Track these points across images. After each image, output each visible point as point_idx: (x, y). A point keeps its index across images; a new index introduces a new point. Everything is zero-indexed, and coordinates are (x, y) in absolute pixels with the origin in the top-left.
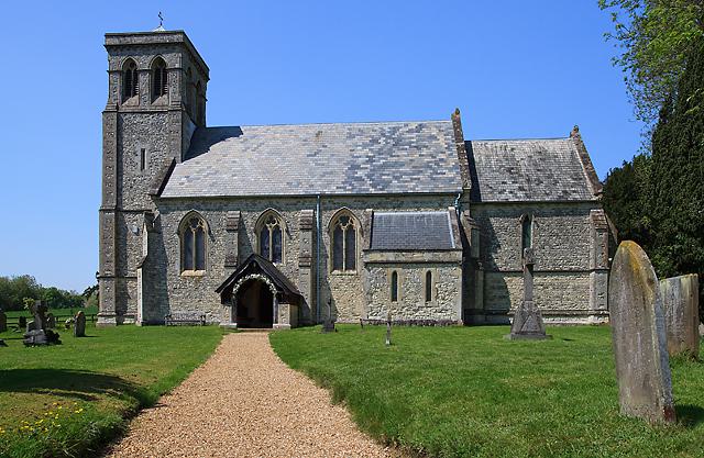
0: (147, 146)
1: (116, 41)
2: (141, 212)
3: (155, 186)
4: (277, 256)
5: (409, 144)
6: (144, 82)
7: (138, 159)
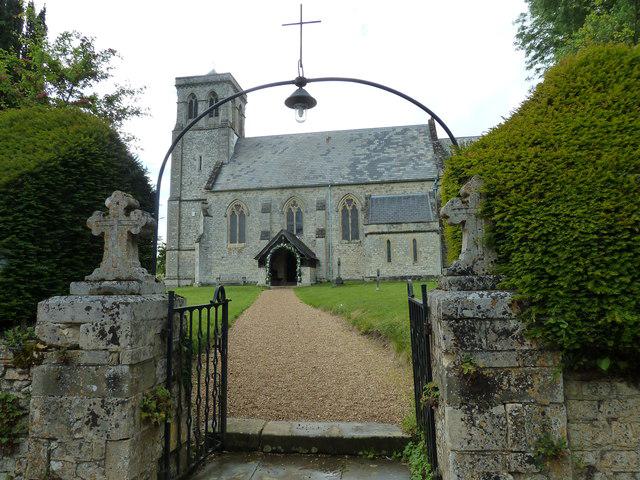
4: (300, 230)
7: (197, 163)
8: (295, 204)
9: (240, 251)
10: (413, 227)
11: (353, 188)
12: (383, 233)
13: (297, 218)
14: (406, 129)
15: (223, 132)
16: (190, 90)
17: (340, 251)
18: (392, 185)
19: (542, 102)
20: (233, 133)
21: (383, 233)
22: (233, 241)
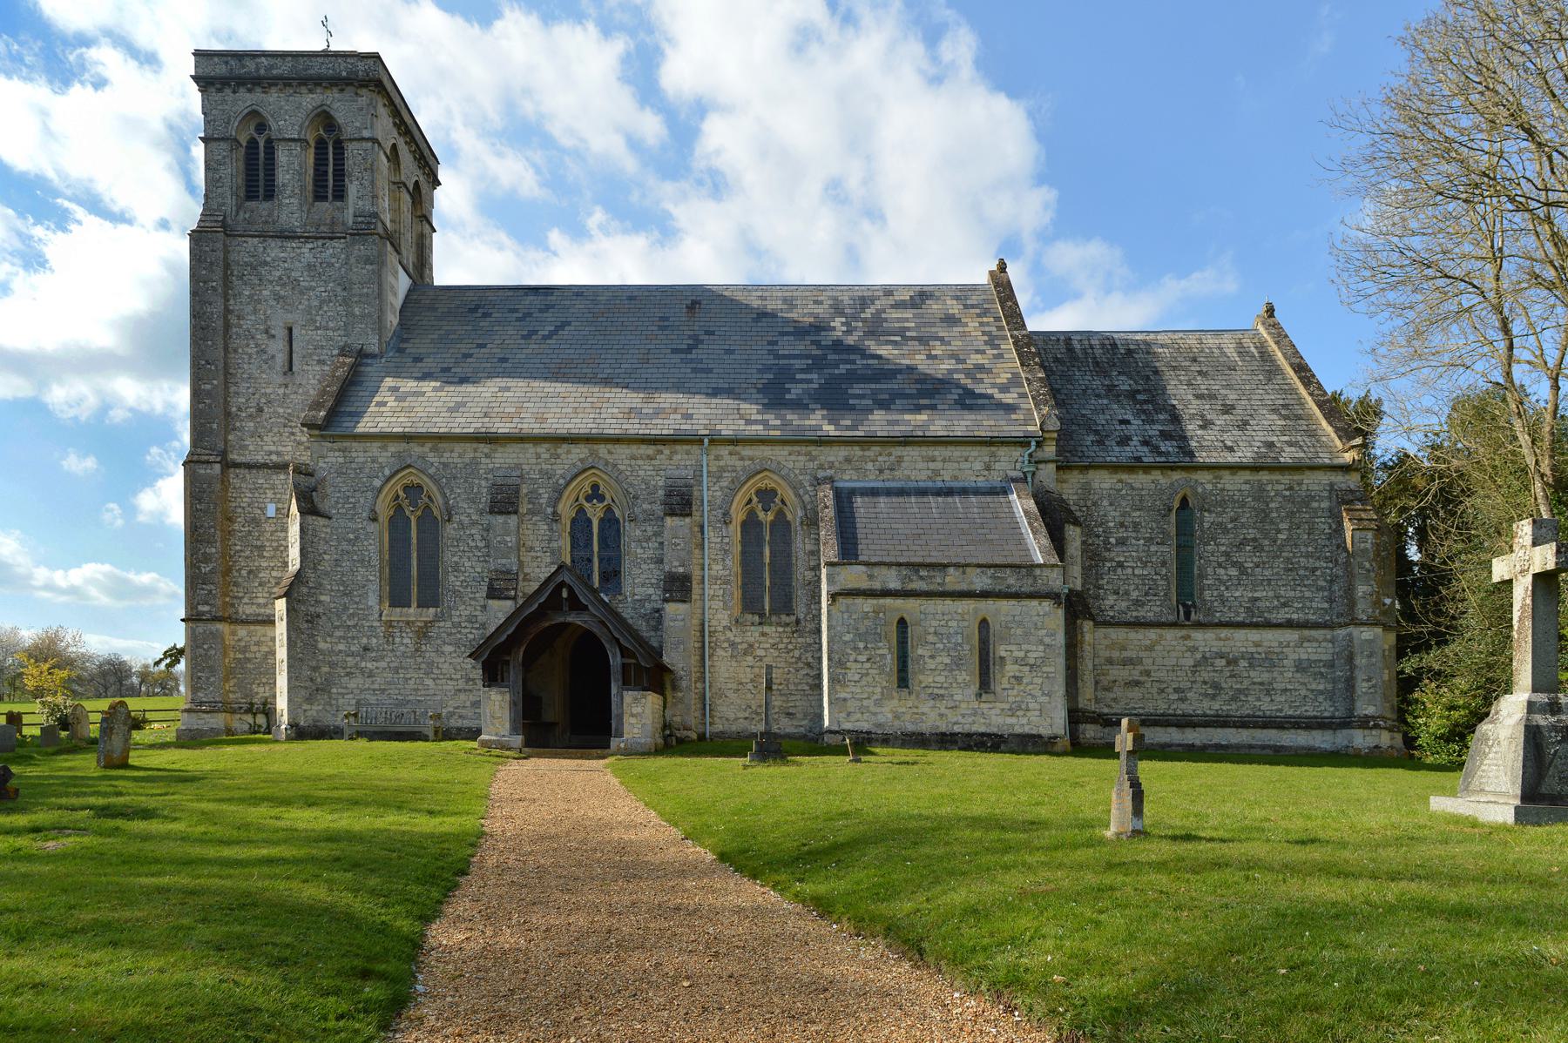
0: (295, 318)
1: (221, 69)
2: (282, 467)
3: (316, 405)
4: (612, 575)
5: (902, 332)
6: (292, 166)
7: (277, 347)
8: (595, 494)
9: (423, 634)
10: (980, 581)
11: (780, 453)
12: (886, 593)
13: (602, 540)
14: (922, 296)
15: (360, 249)
16: (246, 100)
17: (733, 645)
18: (898, 451)
19: (135, 493)
20: (392, 258)
21: (886, 593)
22: (398, 599)
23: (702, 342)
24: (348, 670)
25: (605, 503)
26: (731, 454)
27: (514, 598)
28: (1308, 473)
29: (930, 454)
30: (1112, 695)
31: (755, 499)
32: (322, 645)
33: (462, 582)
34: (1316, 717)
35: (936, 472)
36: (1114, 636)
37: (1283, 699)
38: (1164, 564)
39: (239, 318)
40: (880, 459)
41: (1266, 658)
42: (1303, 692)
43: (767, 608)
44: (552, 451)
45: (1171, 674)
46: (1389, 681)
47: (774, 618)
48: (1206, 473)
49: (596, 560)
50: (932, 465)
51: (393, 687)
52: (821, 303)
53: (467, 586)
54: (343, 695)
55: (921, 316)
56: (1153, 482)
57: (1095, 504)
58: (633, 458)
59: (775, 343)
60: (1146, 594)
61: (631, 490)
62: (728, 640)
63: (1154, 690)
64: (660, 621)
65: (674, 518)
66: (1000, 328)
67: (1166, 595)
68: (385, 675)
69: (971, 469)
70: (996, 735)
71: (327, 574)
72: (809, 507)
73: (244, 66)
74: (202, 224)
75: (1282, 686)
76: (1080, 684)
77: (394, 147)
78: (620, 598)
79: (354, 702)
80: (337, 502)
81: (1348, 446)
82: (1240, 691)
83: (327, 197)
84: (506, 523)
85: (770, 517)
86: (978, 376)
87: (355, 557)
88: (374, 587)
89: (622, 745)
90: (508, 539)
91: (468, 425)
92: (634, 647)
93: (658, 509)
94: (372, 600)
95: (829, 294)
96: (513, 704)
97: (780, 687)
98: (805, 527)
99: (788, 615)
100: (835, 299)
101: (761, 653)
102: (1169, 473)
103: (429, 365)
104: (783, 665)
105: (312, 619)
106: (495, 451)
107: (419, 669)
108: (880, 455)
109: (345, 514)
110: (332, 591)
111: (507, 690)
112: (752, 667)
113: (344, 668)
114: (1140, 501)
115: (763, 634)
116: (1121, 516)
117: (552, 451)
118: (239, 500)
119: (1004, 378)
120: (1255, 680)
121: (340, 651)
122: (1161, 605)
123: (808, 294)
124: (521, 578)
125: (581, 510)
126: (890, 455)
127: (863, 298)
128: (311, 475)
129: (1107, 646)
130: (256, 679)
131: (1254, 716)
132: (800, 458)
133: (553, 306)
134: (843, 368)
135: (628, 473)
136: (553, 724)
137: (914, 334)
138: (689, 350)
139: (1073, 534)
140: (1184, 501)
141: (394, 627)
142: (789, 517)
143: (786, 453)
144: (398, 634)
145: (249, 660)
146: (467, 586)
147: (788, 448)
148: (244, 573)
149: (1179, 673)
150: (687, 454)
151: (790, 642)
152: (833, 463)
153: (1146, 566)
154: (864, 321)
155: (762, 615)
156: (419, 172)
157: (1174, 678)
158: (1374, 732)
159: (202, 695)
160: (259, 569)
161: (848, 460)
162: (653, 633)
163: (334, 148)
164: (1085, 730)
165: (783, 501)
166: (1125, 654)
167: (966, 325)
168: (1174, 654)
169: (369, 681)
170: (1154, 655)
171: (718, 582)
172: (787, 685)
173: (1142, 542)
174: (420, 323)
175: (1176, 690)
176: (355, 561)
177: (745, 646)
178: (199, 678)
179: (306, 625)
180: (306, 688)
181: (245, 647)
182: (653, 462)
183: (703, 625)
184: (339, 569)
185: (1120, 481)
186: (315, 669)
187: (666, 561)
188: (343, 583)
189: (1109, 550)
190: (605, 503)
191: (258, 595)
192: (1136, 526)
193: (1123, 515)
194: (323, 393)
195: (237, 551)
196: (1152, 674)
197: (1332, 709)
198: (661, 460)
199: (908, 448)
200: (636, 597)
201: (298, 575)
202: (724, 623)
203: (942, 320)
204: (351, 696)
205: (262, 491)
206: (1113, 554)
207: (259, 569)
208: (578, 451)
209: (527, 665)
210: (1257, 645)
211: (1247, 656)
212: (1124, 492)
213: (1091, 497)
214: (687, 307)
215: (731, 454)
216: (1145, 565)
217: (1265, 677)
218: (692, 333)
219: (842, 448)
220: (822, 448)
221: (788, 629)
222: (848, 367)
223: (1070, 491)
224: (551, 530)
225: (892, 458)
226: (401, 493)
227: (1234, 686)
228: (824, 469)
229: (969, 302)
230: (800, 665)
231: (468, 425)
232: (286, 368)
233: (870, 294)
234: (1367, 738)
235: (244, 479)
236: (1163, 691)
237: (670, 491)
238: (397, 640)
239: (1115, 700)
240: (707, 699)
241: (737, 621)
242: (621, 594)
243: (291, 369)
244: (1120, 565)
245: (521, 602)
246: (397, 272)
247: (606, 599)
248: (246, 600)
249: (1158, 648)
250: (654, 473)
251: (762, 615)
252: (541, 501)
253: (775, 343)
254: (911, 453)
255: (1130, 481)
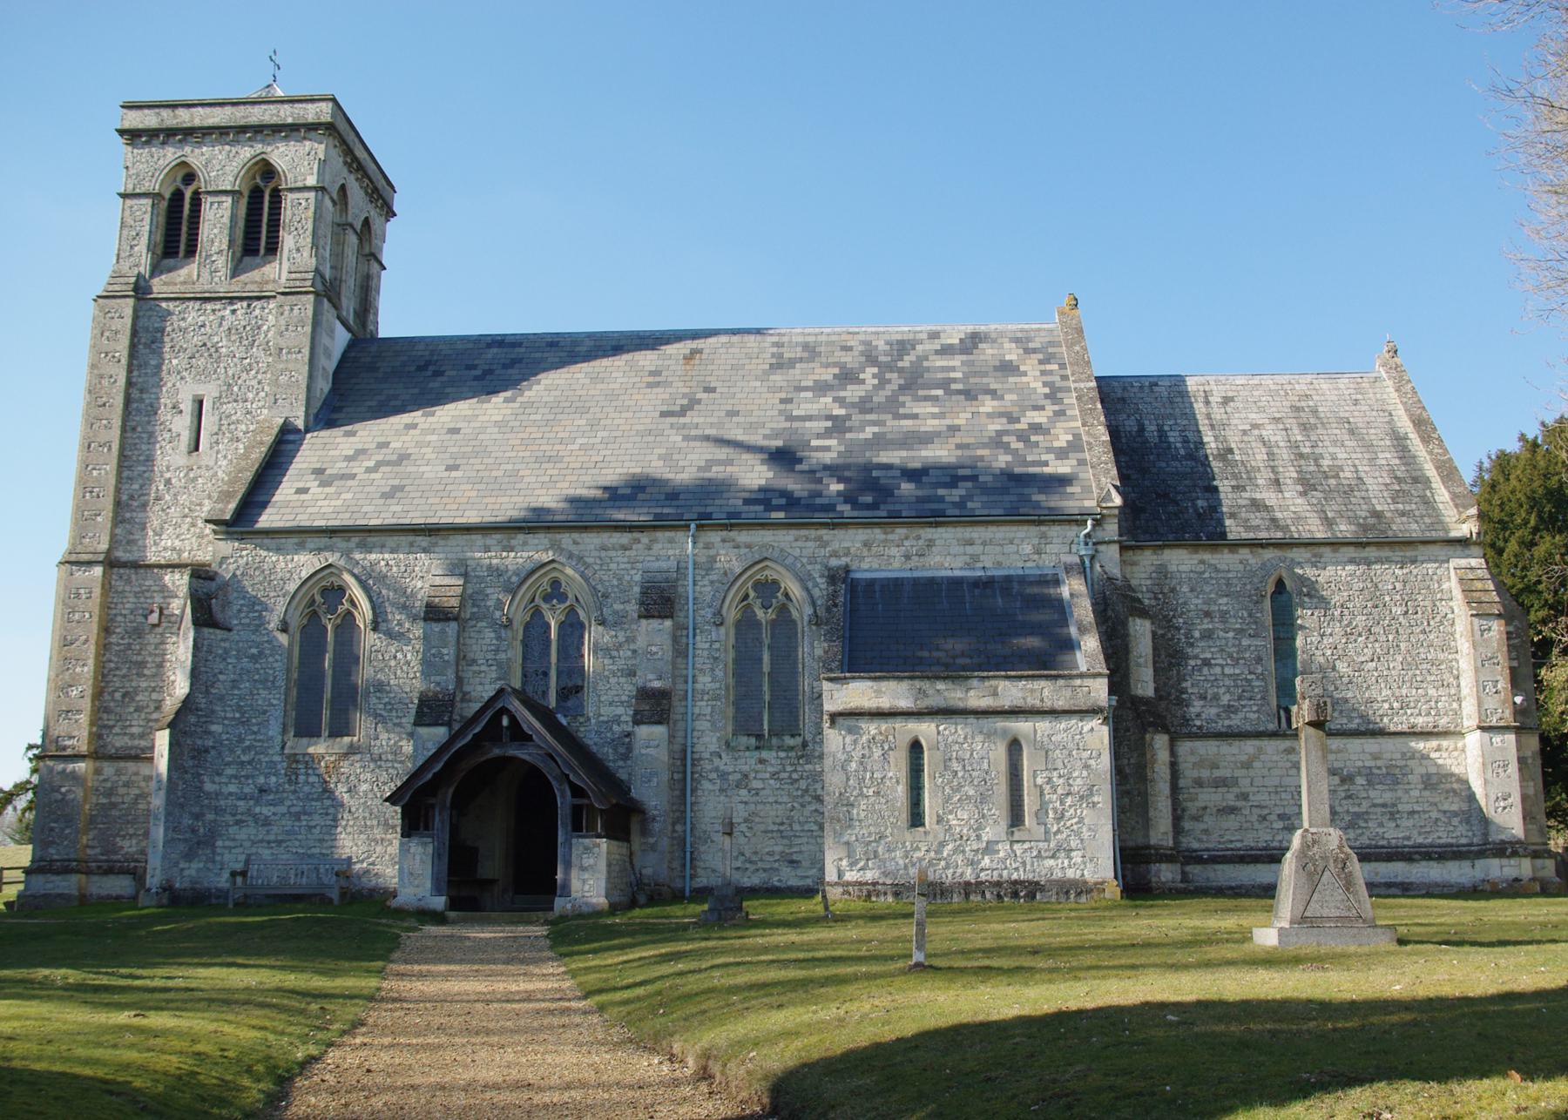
5: (945, 384)
17: (723, 776)
23: (699, 402)
24: (239, 817)
25: (568, 603)
26: (724, 541)
27: (449, 724)
28: (1421, 548)
29: (967, 535)
30: (1202, 826)
31: (752, 594)
32: (208, 787)
33: (385, 704)
34: (1451, 845)
35: (975, 558)
36: (1202, 752)
37: (1410, 823)
38: (1259, 660)
39: (142, 391)
40: (906, 543)
41: (1388, 774)
42: (1434, 815)
43: (766, 727)
44: (505, 543)
45: (1273, 796)
46: (1536, 795)
47: (774, 741)
48: (1302, 550)
49: (553, 674)
50: (969, 550)
51: (292, 837)
52: (850, 349)
53: (391, 710)
54: (230, 848)
55: (971, 363)
56: (1241, 562)
57: (1173, 590)
58: (604, 548)
59: (789, 401)
60: (1240, 698)
61: (599, 587)
62: (717, 770)
63: (1254, 818)
64: (629, 748)
65: (651, 621)
66: (1064, 378)
67: (1263, 698)
68: (284, 823)
69: (1017, 552)
70: (1030, 883)
71: (221, 698)
72: (819, 602)
73: (175, 117)
74: (111, 288)
75: (1408, 808)
76: (1152, 813)
77: (343, 188)
78: (582, 720)
79: (242, 858)
80: (240, 611)
81: (1464, 516)
82: (1358, 815)
83: (258, 251)
84: (443, 632)
85: (771, 614)
86: (1033, 438)
87: (257, 677)
88: (279, 713)
89: (569, 906)
90: (445, 651)
91: (404, 515)
92: (586, 783)
93: (633, 608)
94: (274, 730)
95: (862, 337)
96: (437, 855)
97: (782, 828)
98: (814, 628)
99: (793, 736)
100: (868, 343)
101: (756, 784)
102: (1260, 550)
103: (363, 440)
104: (785, 799)
105: (200, 753)
106: (436, 544)
107: (327, 814)
108: (907, 538)
109: (249, 625)
110: (226, 718)
111: (430, 840)
112: (746, 803)
113: (234, 815)
114: (1228, 585)
115: (762, 761)
116: (1204, 603)
117: (505, 543)
118: (120, 606)
119: (1063, 440)
120: (1375, 801)
121: (230, 794)
122: (1258, 711)
123: (834, 338)
124: (458, 699)
125: (537, 613)
126: (918, 538)
127: (901, 343)
128: (212, 578)
129: (1194, 764)
130: (121, 829)
131: (1377, 847)
132: (810, 544)
133: (520, 361)
134: (870, 431)
135: (597, 567)
136: (492, 882)
137: (959, 386)
138: (683, 412)
139: (1141, 632)
140: (1280, 584)
141: (297, 762)
142: (795, 614)
143: (791, 538)
144: (303, 771)
145: (114, 805)
146: (391, 710)
147: (794, 533)
148: (118, 696)
149: (1284, 796)
150: (670, 542)
151: (795, 771)
152: (848, 548)
153: (1238, 663)
154: (901, 371)
155: (759, 737)
156: (370, 207)
157: (1278, 802)
158: (1512, 862)
159: (53, 851)
160: (136, 691)
161: (867, 544)
162: (621, 763)
163: (271, 196)
164: (1159, 871)
165: (787, 595)
166: (1217, 773)
167: (1025, 374)
168: (1276, 772)
169: (263, 830)
170: (1252, 773)
171: (706, 697)
172: (791, 825)
173: (1231, 634)
174: (357, 387)
175: (1281, 817)
176: (256, 681)
177: (738, 776)
178: (52, 829)
179: (191, 763)
180: (185, 840)
181: (111, 789)
182: (627, 553)
183: (684, 751)
184: (236, 692)
185: (1202, 562)
186: (197, 817)
187: (639, 673)
188: (239, 708)
189: (1192, 645)
190: (568, 603)
191: (134, 723)
192: (1224, 615)
193: (1208, 602)
194: (231, 482)
195: (111, 670)
196: (1251, 797)
197: (1470, 834)
198: (638, 551)
199: (940, 530)
200: (601, 719)
201: (187, 703)
202: (713, 748)
203: (996, 369)
204: (241, 850)
205: (148, 595)
206: (1197, 651)
207: (136, 691)
208: (536, 541)
209: (460, 805)
210: (1375, 757)
211: (1364, 771)
212: (1207, 575)
213: (1168, 581)
214: (685, 358)
215: (724, 541)
216: (1236, 662)
217: (1388, 797)
218: (687, 390)
219: (860, 531)
220: (836, 532)
221: (792, 754)
222: (876, 429)
223: (1143, 575)
224: (499, 638)
225: (921, 542)
226: (318, 598)
227: (1351, 810)
228: (839, 557)
229: (1031, 345)
230: (808, 799)
231: (404, 515)
232: (192, 447)
233: (911, 337)
234: (1505, 869)
235: (129, 581)
236: (1264, 818)
237: (648, 588)
238: (302, 778)
239: (1206, 831)
240: (688, 845)
241: (728, 744)
242: (582, 715)
243: (197, 448)
244: (1207, 663)
245: (456, 727)
246: (332, 331)
247: (564, 722)
248: (117, 730)
249: (1256, 764)
250: (629, 566)
251: (759, 737)
252: (489, 603)
253: (789, 401)
254: (944, 535)
255: (1213, 562)
